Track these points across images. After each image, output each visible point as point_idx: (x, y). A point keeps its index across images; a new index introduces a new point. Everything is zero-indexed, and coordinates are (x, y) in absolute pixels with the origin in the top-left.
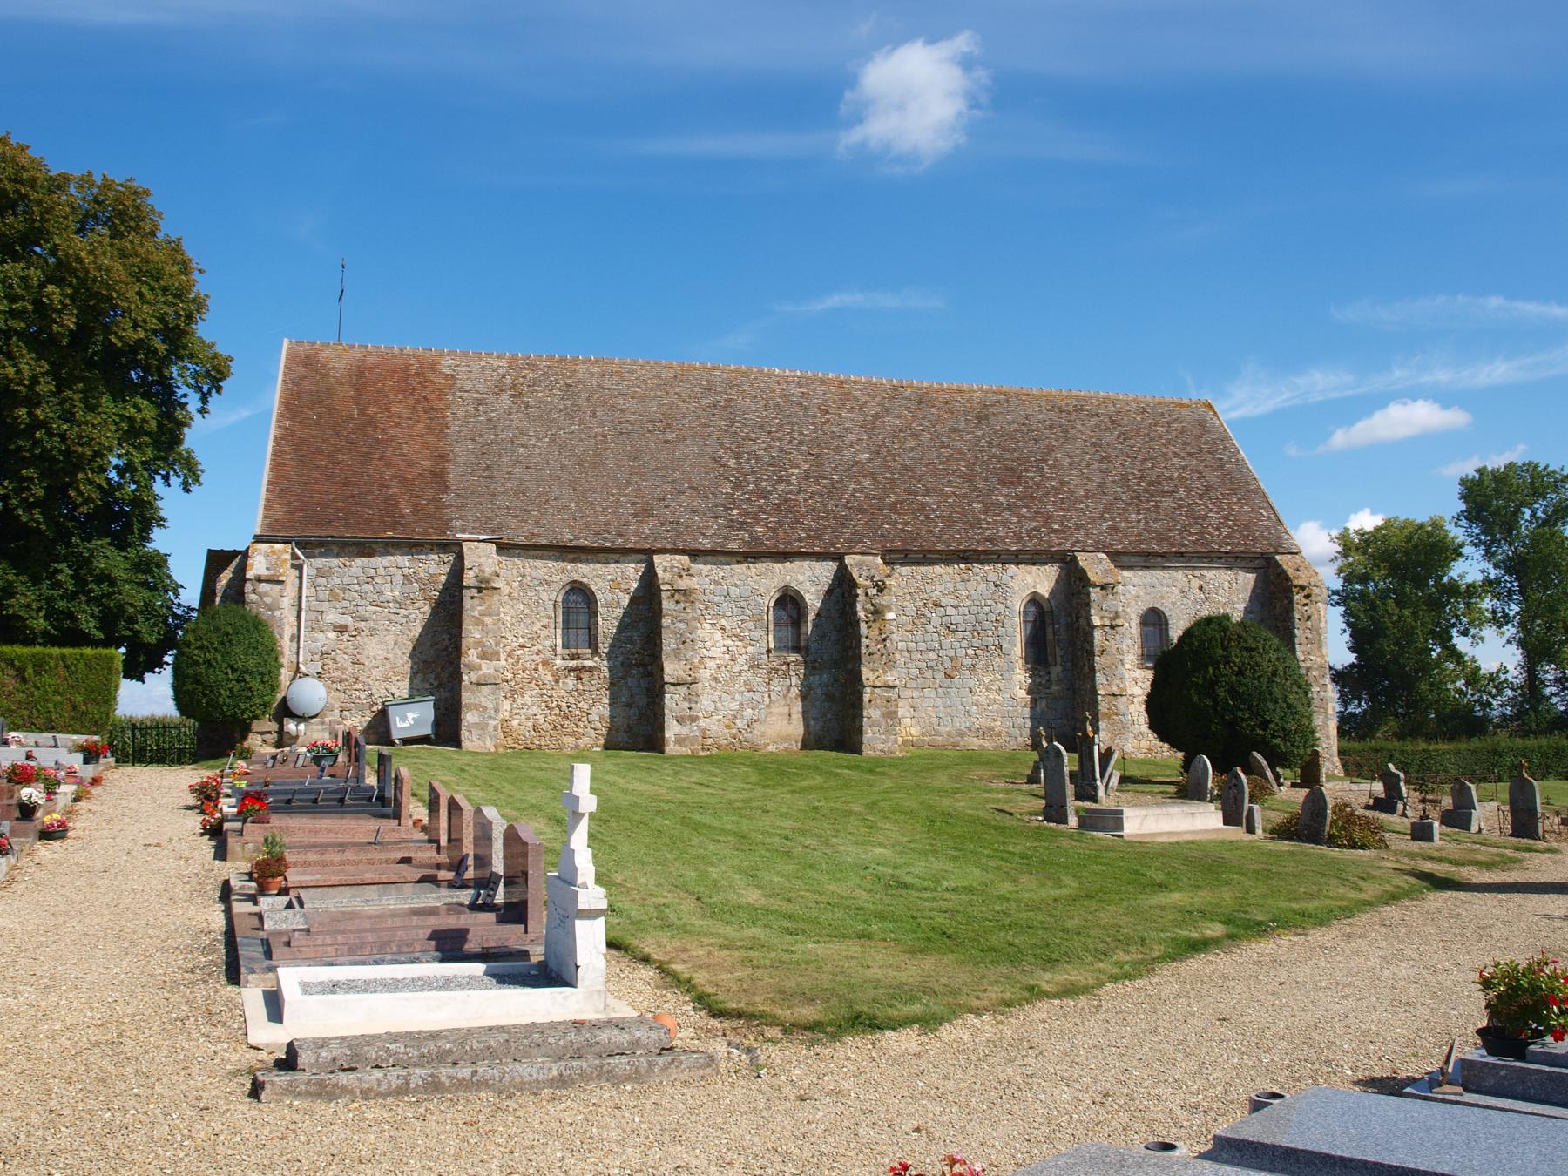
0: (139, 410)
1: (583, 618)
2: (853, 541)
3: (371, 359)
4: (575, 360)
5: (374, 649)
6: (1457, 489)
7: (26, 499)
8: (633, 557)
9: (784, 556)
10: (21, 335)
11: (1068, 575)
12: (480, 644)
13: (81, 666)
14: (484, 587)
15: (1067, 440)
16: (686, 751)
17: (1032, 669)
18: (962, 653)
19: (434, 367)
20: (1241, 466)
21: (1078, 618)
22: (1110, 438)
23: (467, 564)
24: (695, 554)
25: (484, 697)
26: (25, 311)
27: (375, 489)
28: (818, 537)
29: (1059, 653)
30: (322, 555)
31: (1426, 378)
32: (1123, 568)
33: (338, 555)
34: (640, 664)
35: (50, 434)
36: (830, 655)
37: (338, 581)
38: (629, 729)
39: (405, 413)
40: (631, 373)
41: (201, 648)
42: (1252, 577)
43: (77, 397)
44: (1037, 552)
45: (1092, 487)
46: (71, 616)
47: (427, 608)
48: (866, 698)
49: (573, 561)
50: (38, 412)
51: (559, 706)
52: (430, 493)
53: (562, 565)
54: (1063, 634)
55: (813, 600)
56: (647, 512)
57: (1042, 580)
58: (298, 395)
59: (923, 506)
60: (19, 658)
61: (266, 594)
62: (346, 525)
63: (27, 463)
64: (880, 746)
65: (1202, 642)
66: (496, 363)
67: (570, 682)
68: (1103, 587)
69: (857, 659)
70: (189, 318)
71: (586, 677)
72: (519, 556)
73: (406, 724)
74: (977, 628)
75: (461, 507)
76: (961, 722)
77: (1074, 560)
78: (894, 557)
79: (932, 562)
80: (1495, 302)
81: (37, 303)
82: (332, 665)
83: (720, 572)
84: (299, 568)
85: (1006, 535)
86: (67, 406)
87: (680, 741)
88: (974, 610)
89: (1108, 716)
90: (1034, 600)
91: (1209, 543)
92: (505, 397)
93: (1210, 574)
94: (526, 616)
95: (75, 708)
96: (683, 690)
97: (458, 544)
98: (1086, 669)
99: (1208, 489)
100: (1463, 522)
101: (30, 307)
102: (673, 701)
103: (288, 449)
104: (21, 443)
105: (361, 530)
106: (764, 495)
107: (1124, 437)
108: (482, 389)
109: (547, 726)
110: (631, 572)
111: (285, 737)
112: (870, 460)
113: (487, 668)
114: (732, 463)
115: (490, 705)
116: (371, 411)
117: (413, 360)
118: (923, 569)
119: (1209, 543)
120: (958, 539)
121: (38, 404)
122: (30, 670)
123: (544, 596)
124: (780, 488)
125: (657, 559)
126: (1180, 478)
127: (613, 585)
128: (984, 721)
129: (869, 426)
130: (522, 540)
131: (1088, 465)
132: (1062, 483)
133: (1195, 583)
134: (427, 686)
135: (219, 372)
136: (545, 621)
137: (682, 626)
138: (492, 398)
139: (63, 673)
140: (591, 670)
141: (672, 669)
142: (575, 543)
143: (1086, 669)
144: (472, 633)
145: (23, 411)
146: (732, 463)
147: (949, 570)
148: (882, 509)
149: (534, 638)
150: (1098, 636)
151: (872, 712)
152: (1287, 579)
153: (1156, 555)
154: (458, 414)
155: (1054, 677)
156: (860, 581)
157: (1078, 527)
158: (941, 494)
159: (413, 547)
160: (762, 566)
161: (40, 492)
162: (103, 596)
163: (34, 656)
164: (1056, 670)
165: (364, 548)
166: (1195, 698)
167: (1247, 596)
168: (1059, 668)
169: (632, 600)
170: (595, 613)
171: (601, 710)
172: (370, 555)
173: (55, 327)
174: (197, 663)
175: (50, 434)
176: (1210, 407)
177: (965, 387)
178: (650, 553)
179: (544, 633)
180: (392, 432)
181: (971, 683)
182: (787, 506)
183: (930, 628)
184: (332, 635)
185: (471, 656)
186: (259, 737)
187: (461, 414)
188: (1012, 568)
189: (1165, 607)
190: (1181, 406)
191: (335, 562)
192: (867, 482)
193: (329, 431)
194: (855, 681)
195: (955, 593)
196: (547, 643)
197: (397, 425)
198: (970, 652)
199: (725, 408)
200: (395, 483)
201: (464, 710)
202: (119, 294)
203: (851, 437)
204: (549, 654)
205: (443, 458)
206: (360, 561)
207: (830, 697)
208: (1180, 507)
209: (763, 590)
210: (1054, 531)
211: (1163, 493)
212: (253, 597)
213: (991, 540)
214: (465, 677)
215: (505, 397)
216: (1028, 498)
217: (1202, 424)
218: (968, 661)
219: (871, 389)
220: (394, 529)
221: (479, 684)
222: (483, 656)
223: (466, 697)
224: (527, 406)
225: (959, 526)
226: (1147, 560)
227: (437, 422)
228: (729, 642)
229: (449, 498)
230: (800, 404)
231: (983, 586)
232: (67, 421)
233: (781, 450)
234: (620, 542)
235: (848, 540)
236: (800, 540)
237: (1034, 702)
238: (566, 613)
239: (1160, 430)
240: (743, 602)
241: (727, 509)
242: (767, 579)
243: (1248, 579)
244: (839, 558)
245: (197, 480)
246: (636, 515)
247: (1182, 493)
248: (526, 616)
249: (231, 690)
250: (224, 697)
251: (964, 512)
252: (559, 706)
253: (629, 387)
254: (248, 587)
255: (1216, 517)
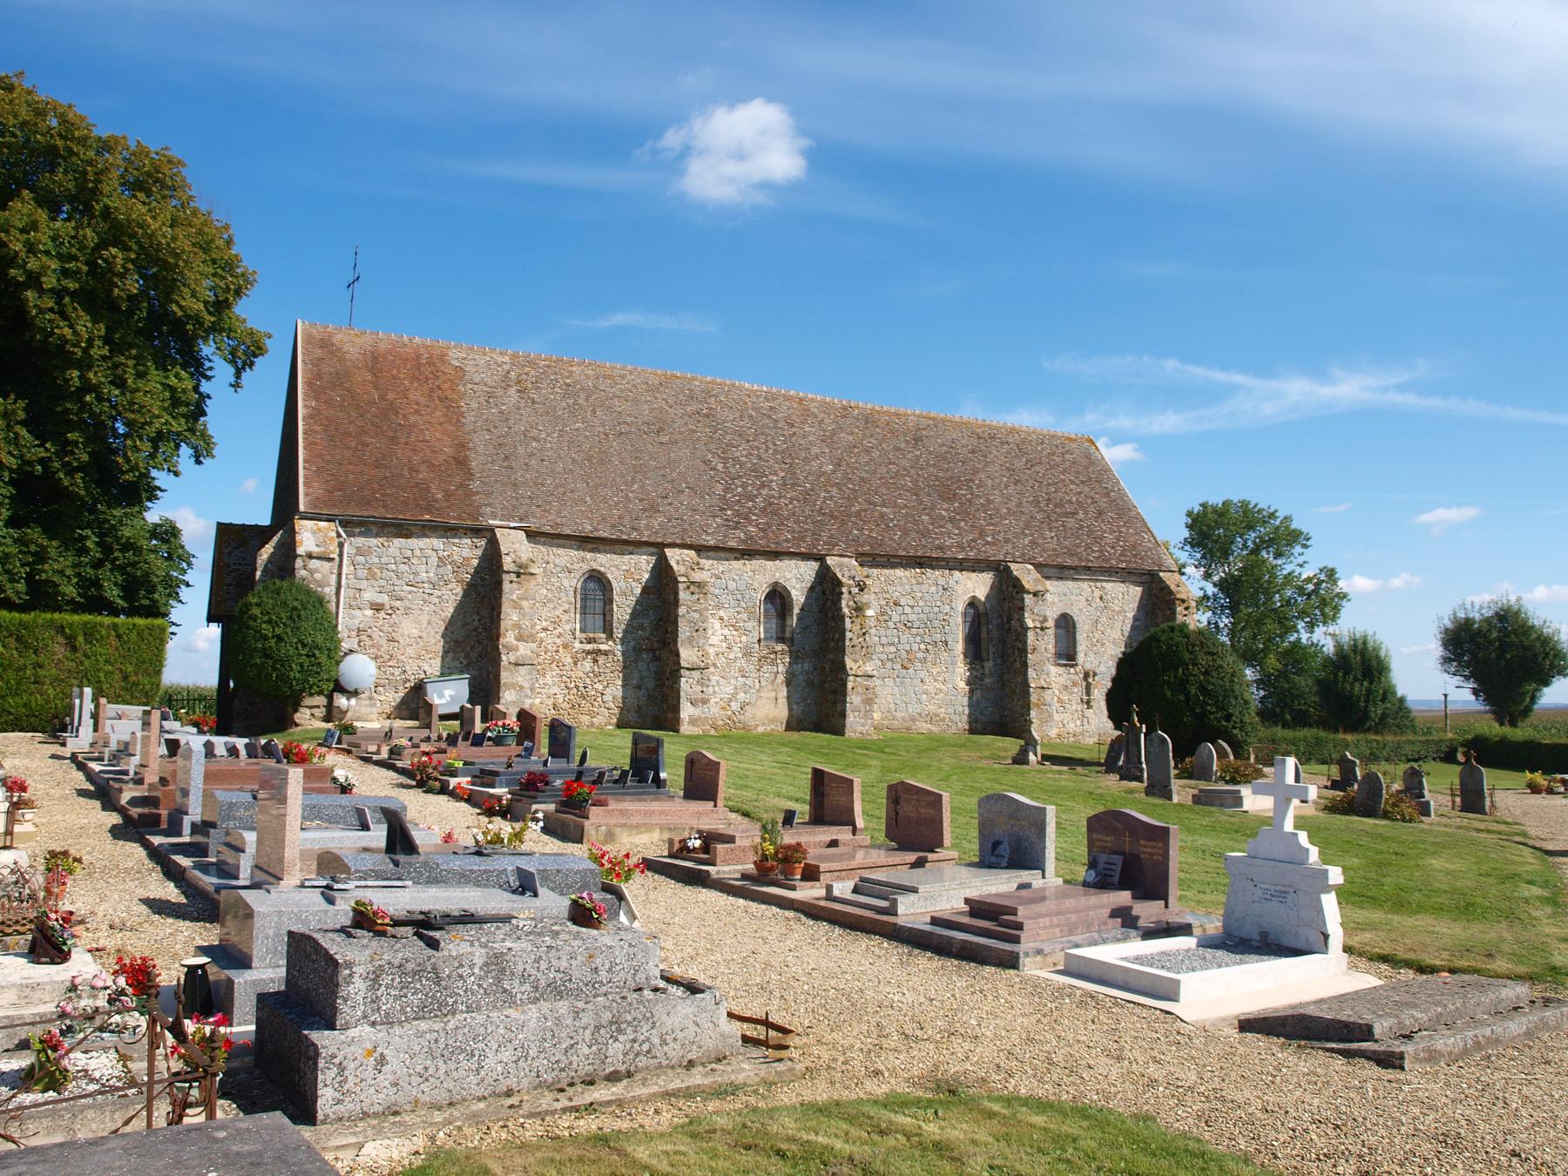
0: (180, 380)
1: (599, 604)
2: (832, 544)
3: (383, 346)
4: (570, 363)
5: (408, 628)
6: (1185, 519)
7: (69, 463)
8: (646, 549)
9: (775, 555)
10: (73, 294)
11: (1000, 582)
12: (517, 626)
13: (134, 636)
14: (522, 572)
15: (987, 464)
16: (696, 731)
17: (971, 663)
18: (915, 647)
19: (442, 357)
20: (1123, 495)
21: (1009, 620)
22: (1020, 464)
23: (503, 550)
24: (700, 549)
25: (522, 676)
26: (79, 271)
27: (406, 473)
28: (802, 539)
29: (992, 650)
30: (361, 534)
31: (1112, 424)
32: (1048, 578)
33: (377, 536)
34: (651, 650)
35: (100, 399)
36: (816, 647)
37: (376, 560)
38: (639, 709)
39: (423, 400)
40: (623, 377)
41: (269, 622)
42: (1139, 589)
43: (131, 363)
44: (978, 561)
45: (1012, 505)
46: (96, 583)
47: (459, 590)
48: (850, 685)
49: (591, 551)
50: (91, 375)
51: (577, 687)
52: (457, 479)
53: (582, 553)
54: (995, 634)
55: (798, 596)
56: (653, 509)
57: (978, 586)
58: (319, 376)
59: (882, 515)
60: (71, 625)
61: (316, 571)
62: (385, 506)
63: (73, 426)
64: (859, 729)
65: (1169, 646)
66: (500, 359)
67: (588, 665)
68: (1035, 594)
69: (842, 650)
70: (238, 293)
71: (601, 659)
72: (544, 544)
73: (443, 701)
74: (927, 624)
75: (488, 494)
76: (914, 709)
77: (1008, 570)
78: (875, 559)
79: (893, 566)
80: (1171, 364)
81: (92, 264)
82: (368, 642)
83: (721, 566)
84: (341, 545)
85: (951, 541)
86: (119, 371)
87: (693, 721)
88: (926, 609)
89: (1037, 706)
90: (973, 603)
91: (1107, 560)
92: (512, 391)
93: (1108, 586)
94: (550, 601)
95: (125, 678)
96: (696, 674)
97: (491, 530)
98: (1018, 665)
99: (1100, 513)
100: (1188, 548)
101: (85, 268)
102: (688, 685)
103: (317, 428)
104: (69, 405)
105: (400, 512)
106: (751, 498)
107: (1030, 464)
108: (490, 383)
109: (565, 705)
110: (644, 564)
111: (335, 711)
112: (834, 472)
113: (524, 650)
114: (720, 467)
115: (526, 685)
116: (390, 396)
117: (422, 350)
118: (887, 572)
119: (1107, 560)
120: (913, 547)
121: (90, 367)
122: (81, 639)
123: (566, 583)
124: (764, 492)
125: (669, 552)
126: (1078, 502)
127: (628, 575)
128: (932, 708)
129: (829, 440)
130: (547, 529)
131: (1007, 487)
132: (988, 500)
133: (1097, 593)
134: (457, 664)
135: (259, 348)
136: (566, 606)
137: (696, 615)
138: (500, 392)
139: (114, 642)
140: (606, 653)
141: (687, 655)
142: (596, 534)
143: (1018, 665)
144: (510, 616)
145: (76, 373)
146: (720, 467)
147: (907, 573)
148: (849, 516)
149: (557, 623)
150: (1030, 635)
151: (854, 699)
152: (1171, 592)
153: (1070, 568)
154: (471, 405)
155: (987, 670)
156: (844, 580)
157: (1007, 541)
158: (896, 505)
159: (448, 531)
160: (757, 563)
161: (85, 457)
162: (129, 564)
163: (85, 624)
164: (989, 665)
165: (402, 529)
166: (1169, 694)
167: (1135, 605)
168: (991, 663)
169: (645, 590)
170: (611, 601)
171: (614, 691)
172: (407, 537)
173: (116, 291)
174: (266, 638)
175: (100, 399)
176: (1093, 443)
177: (902, 410)
178: (663, 546)
179: (565, 617)
180: (413, 418)
181: (922, 674)
182: (770, 509)
183: (891, 624)
184: (369, 613)
185: (508, 638)
186: (308, 711)
187: (474, 405)
188: (957, 574)
189: (1074, 612)
190: (1070, 439)
191: (374, 541)
192: (835, 491)
193: (353, 414)
194: (840, 670)
195: (911, 593)
196: (568, 627)
197: (416, 412)
198: (923, 647)
199: (707, 416)
200: (423, 467)
201: (502, 689)
202: (186, 262)
203: (815, 450)
204: (569, 637)
205: (463, 446)
206: (398, 542)
207: (810, 684)
208: (1082, 527)
209: (756, 585)
210: (988, 543)
211: (1067, 514)
212: (304, 573)
213: (940, 548)
214: (504, 658)
215: (512, 391)
216: (964, 512)
217: (1088, 456)
218: (920, 655)
219: (827, 407)
220: (430, 513)
221: (517, 665)
222: (520, 638)
223: (505, 676)
224: (533, 402)
225: (914, 535)
226: (1062, 572)
227: (454, 414)
228: (726, 631)
229: (475, 485)
230: (769, 417)
231: (933, 589)
232: (117, 386)
233: (760, 458)
234: (634, 535)
235: (827, 543)
236: (787, 541)
237: (971, 691)
238: (584, 600)
239: (1058, 460)
240: (739, 596)
241: (722, 509)
242: (759, 575)
243: (1136, 591)
244: (820, 559)
245: (210, 454)
246: (644, 510)
247: (1081, 515)
248: (550, 601)
249: (301, 665)
250: (295, 673)
251: (916, 522)
252: (577, 687)
253: (622, 391)
254: (299, 563)
255: (1110, 538)
